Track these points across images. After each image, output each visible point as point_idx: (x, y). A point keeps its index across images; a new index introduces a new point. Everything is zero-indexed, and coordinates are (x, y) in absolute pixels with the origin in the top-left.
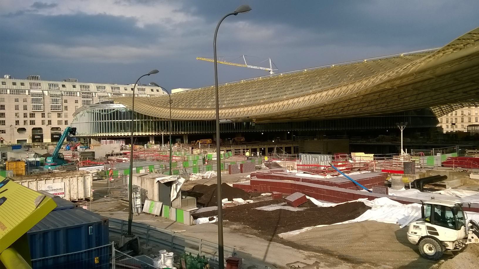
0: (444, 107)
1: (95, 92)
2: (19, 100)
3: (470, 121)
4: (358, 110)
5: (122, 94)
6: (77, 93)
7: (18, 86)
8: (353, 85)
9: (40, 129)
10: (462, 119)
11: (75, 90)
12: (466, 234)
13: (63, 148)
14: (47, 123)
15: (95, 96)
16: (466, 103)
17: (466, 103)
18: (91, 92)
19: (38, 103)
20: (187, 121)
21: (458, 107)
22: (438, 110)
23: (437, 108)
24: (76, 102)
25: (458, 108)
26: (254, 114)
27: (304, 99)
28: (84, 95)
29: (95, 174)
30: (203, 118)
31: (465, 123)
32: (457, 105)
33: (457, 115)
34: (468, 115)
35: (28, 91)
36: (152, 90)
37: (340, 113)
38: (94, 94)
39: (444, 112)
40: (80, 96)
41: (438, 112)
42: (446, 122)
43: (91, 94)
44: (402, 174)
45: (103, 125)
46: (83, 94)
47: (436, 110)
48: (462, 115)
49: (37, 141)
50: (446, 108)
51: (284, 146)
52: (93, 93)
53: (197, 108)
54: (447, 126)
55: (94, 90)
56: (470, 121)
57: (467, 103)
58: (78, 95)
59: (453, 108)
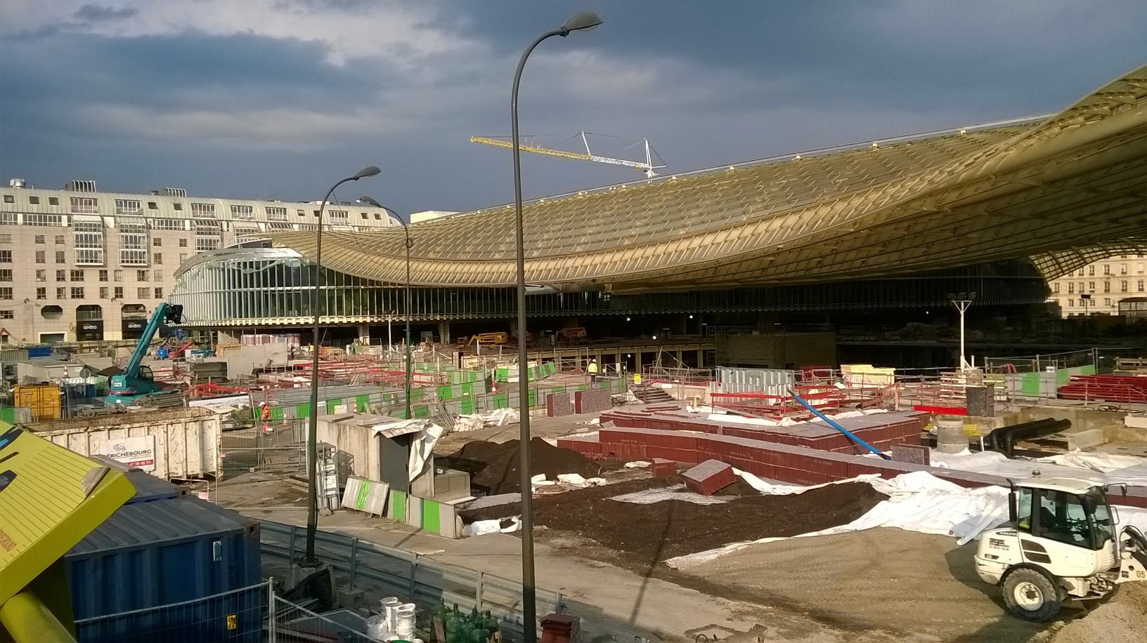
0: (1063, 257)
1: (226, 221)
2: (45, 238)
3: (1126, 290)
5: (292, 224)
6: (184, 222)
7: (44, 207)
8: (846, 204)
9: (96, 308)
10: (1107, 284)
11: (179, 214)
12: (1117, 560)
13: (152, 354)
14: (112, 293)
15: (228, 230)
16: (1116, 247)
17: (1116, 247)
18: (218, 220)
19: (91, 246)
20: (448, 290)
21: (1096, 256)
22: (1050, 263)
23: (1047, 258)
24: (183, 243)
25: (1096, 258)
26: (609, 272)
27: (727, 238)
28: (202, 226)
30: (485, 282)
32: (1094, 252)
33: (1093, 274)
34: (1120, 275)
35: (66, 217)
36: (364, 216)
37: (815, 271)
38: (225, 224)
39: (1064, 269)
40: (191, 230)
41: (1048, 267)
42: (1067, 293)
43: (217, 225)
44: (962, 417)
45: (247, 299)
46: (198, 224)
47: (1043, 264)
48: (1107, 276)
49: (89, 336)
50: (1067, 258)
51: (679, 349)
54: (1070, 300)
56: (1124, 290)
59: (1084, 259)
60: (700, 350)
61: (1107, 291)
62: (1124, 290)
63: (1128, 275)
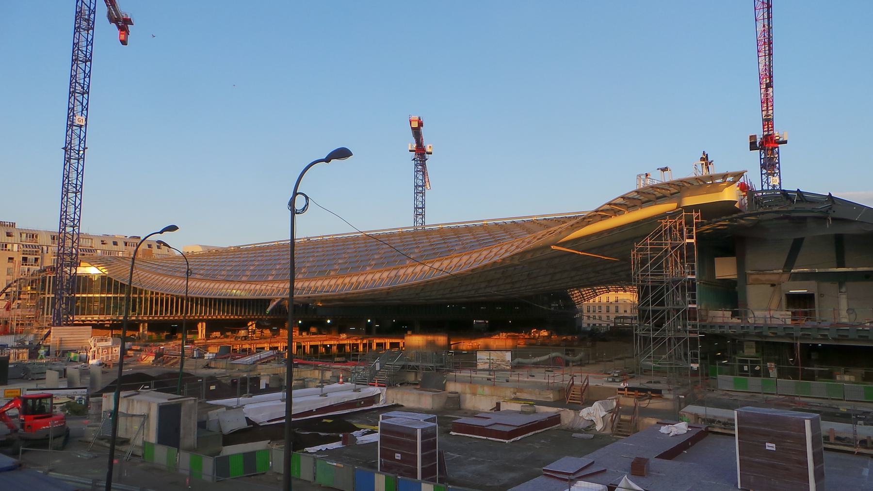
0: (584, 291)
1: (47, 246)
3: (618, 311)
4: (473, 292)
5: (96, 250)
6: (13, 246)
15: (47, 253)
16: (613, 287)
17: (613, 287)
18: (40, 245)
20: (237, 300)
21: (602, 291)
23: (576, 292)
27: (397, 273)
28: (27, 249)
29: (62, 405)
30: (262, 295)
31: (612, 313)
32: (612, 288)
37: (448, 296)
38: (45, 248)
39: (585, 298)
40: (18, 251)
42: (587, 312)
43: (39, 248)
46: (81, 251)
47: (575, 294)
50: (587, 292)
52: (44, 247)
53: (258, 280)
54: (607, 316)
55: (43, 242)
56: (617, 311)
57: (631, 287)
58: (16, 247)
59: (596, 293)
60: (320, 345)
61: (608, 311)
62: (617, 311)
63: (618, 303)
